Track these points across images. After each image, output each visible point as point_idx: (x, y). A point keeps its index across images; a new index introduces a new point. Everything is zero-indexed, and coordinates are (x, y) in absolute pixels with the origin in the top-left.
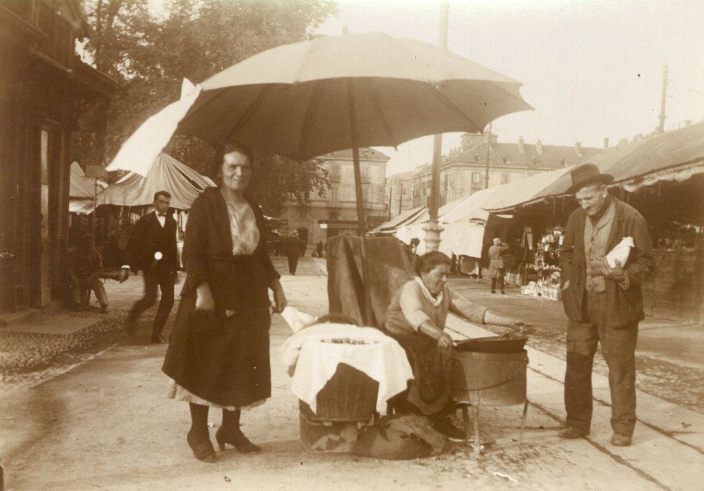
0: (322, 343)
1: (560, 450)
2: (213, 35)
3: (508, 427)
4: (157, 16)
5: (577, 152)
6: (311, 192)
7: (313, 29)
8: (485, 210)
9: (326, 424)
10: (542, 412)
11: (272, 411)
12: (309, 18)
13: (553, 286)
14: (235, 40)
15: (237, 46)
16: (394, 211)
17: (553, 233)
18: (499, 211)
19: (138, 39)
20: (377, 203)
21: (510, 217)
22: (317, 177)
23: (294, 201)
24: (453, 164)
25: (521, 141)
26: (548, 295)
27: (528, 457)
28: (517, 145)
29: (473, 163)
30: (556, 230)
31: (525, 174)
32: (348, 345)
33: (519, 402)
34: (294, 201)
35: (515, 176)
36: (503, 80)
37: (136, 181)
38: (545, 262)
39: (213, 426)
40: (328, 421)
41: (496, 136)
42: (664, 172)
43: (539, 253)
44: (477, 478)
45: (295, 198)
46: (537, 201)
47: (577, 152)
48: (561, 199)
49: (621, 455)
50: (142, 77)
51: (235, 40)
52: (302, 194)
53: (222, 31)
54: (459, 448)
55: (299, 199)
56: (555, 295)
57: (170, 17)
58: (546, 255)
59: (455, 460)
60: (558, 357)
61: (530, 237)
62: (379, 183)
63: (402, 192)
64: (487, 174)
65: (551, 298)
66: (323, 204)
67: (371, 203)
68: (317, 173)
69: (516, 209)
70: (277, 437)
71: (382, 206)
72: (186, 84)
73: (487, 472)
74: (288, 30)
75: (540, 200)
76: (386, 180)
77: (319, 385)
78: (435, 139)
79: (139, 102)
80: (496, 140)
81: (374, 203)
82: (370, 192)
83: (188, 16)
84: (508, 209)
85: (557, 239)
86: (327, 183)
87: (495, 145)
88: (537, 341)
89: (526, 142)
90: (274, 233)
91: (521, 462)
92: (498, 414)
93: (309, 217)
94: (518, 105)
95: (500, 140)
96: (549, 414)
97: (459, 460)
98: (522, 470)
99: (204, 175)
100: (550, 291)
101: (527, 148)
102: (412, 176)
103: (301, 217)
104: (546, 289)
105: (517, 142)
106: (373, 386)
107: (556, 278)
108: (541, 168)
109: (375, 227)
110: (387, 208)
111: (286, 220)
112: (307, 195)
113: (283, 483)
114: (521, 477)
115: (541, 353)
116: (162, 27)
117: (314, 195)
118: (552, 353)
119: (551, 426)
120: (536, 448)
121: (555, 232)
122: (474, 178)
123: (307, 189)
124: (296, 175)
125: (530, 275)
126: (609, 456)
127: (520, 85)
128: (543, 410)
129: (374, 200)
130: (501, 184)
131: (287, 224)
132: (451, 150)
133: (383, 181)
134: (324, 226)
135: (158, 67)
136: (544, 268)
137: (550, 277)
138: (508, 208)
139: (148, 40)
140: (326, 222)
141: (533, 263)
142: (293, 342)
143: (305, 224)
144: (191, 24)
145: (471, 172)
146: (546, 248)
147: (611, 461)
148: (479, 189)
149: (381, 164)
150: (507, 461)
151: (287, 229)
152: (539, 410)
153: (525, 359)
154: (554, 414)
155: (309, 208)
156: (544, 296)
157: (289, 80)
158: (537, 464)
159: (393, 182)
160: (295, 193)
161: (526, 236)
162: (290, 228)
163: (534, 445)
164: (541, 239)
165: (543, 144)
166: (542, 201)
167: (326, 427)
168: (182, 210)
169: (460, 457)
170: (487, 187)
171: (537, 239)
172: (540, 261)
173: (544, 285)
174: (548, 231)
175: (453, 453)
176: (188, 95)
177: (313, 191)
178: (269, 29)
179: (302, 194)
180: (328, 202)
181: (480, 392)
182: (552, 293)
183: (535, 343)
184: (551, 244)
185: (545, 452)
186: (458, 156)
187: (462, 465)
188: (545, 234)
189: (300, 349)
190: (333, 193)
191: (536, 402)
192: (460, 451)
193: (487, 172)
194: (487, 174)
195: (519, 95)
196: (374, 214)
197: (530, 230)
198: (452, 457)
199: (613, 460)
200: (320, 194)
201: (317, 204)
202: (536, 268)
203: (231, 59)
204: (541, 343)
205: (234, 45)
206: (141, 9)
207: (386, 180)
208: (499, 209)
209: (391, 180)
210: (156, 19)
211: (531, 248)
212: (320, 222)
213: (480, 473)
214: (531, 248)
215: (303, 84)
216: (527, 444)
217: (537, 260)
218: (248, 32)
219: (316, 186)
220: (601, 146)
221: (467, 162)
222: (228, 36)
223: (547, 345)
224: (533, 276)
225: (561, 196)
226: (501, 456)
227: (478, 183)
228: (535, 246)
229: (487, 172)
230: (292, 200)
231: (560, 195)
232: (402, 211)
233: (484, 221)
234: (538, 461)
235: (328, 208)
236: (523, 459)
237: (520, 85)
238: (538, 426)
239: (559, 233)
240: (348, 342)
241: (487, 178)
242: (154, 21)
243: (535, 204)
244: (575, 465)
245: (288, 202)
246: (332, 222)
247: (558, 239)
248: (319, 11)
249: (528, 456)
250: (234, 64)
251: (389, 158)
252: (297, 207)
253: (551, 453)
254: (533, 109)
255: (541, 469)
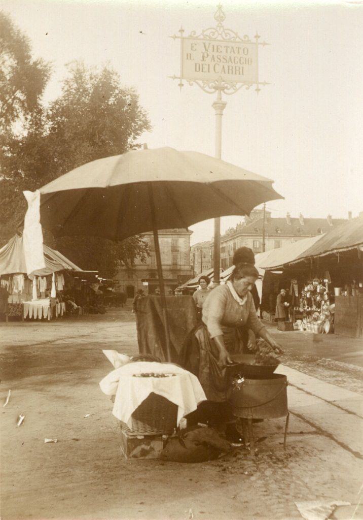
0: (134, 377)
1: (314, 449)
2: (59, 147)
3: (276, 433)
4: (18, 134)
5: (329, 223)
6: (135, 259)
7: (133, 140)
8: (262, 268)
9: (139, 437)
10: (302, 420)
11: (102, 428)
12: (129, 132)
13: (314, 323)
14: (75, 150)
15: (78, 154)
16: (197, 270)
17: (312, 283)
18: (273, 269)
19: (4, 151)
20: (184, 265)
21: (281, 272)
22: (139, 248)
23: (123, 266)
24: (240, 235)
25: (288, 216)
26: (311, 329)
27: (290, 456)
28: (285, 218)
29: (253, 233)
30: (314, 281)
31: (292, 240)
32: (153, 378)
33: (282, 415)
34: (123, 266)
35: (285, 242)
36: (261, 180)
37: (6, 254)
38: (307, 305)
39: (57, 442)
40: (141, 435)
41: (270, 213)
42: (227, 306)
43: (303, 298)
44: (252, 475)
45: (123, 263)
46: (299, 261)
47: (329, 223)
48: (316, 258)
49: (360, 452)
50: (8, 179)
51: (75, 150)
52: (129, 261)
53: (66, 144)
54: (239, 451)
55: (127, 264)
56: (316, 329)
57: (28, 134)
58: (309, 300)
59: (236, 461)
60: (317, 378)
61: (296, 287)
62: (185, 250)
63: (202, 256)
64: (264, 241)
65: (313, 332)
66: (145, 268)
67: (180, 265)
68: (139, 244)
69: (284, 267)
70: (104, 448)
71: (188, 267)
72: (27, 194)
73: (260, 470)
74: (114, 141)
75: (302, 260)
76: (190, 248)
77: (132, 408)
78: (215, 221)
79: (6, 197)
80: (270, 215)
81: (182, 265)
82: (179, 257)
83: (42, 133)
84: (278, 267)
85: (315, 288)
86: (147, 253)
87: (270, 220)
88: (302, 365)
89: (292, 216)
90: (109, 290)
91: (285, 461)
92: (270, 424)
93: (134, 277)
94: (274, 196)
95: (273, 216)
96: (308, 422)
97: (240, 461)
98: (286, 467)
99: (55, 250)
100: (312, 326)
101: (293, 220)
102: (210, 245)
103: (129, 277)
104: (309, 325)
105: (286, 217)
106: (175, 408)
107: (316, 317)
108: (303, 235)
109: (184, 283)
110: (193, 268)
111: (118, 280)
112: (132, 262)
113: (107, 485)
114: (284, 472)
115: (305, 375)
116: (22, 142)
117: (137, 261)
118: (312, 374)
119: (309, 431)
120: (297, 449)
121: (314, 283)
122: (255, 244)
123: (132, 257)
124: (124, 247)
125: (297, 316)
126: (350, 453)
127: (272, 182)
128: (303, 419)
129: (182, 263)
130: (275, 248)
131: (119, 283)
132: (237, 224)
133: (188, 249)
134: (146, 284)
135: (20, 171)
136: (307, 310)
137: (312, 316)
138: (278, 266)
139: (11, 152)
140: (147, 281)
141: (299, 307)
142: (111, 376)
143: (131, 283)
144: (44, 139)
145: (252, 240)
146: (308, 295)
147: (352, 457)
148: (259, 253)
149: (187, 236)
150: (275, 460)
151: (119, 287)
152: (300, 419)
153: (285, 383)
154: (311, 422)
155: (135, 270)
156: (308, 331)
157: (103, 185)
158: (296, 461)
159: (196, 249)
160: (123, 260)
161: (293, 287)
162: (120, 286)
163: (296, 446)
164: (304, 288)
165: (305, 217)
166: (303, 261)
167: (140, 440)
168: (39, 276)
169: (240, 459)
170: (264, 251)
171: (301, 288)
172: (304, 305)
173: (307, 322)
174: (308, 282)
175: (235, 456)
176: (33, 200)
177: (137, 258)
178: (101, 141)
179: (129, 261)
180: (148, 265)
181: (253, 409)
182: (314, 328)
183: (300, 367)
184: (312, 292)
185: (303, 452)
186: (242, 228)
187: (241, 465)
188: (307, 284)
189: (118, 381)
190: (152, 259)
191: (299, 413)
192: (239, 453)
193: (264, 238)
194: (264, 241)
195: (272, 188)
196: (182, 274)
197: (296, 282)
198: (234, 459)
199: (353, 455)
200: (142, 260)
201: (140, 268)
202: (301, 310)
203: (74, 164)
204: (305, 367)
205: (75, 154)
206: (6, 130)
207: (190, 248)
208: (272, 267)
209: (194, 248)
210: (17, 137)
211: (297, 295)
212: (143, 281)
213: (254, 471)
214: (297, 295)
215: (113, 187)
216: (290, 446)
217: (301, 304)
218: (85, 144)
219: (138, 254)
220: (346, 217)
221: (247, 233)
222: (71, 147)
223: (310, 368)
224: (300, 316)
225: (316, 257)
226: (270, 457)
227: (258, 248)
228: (300, 293)
229: (264, 238)
230: (121, 266)
231: (315, 256)
232: (203, 270)
233: (262, 276)
234: (298, 459)
235: (147, 270)
236: (287, 458)
237: (272, 182)
238: (299, 431)
239: (317, 283)
240: (153, 375)
241: (264, 244)
242: (16, 138)
243: (299, 263)
244: (325, 461)
245: (119, 266)
246: (152, 280)
247: (316, 288)
248: (137, 127)
249: (290, 455)
250: (76, 168)
251: (192, 232)
252: (124, 270)
253: (307, 452)
254: (284, 198)
255: (299, 465)
